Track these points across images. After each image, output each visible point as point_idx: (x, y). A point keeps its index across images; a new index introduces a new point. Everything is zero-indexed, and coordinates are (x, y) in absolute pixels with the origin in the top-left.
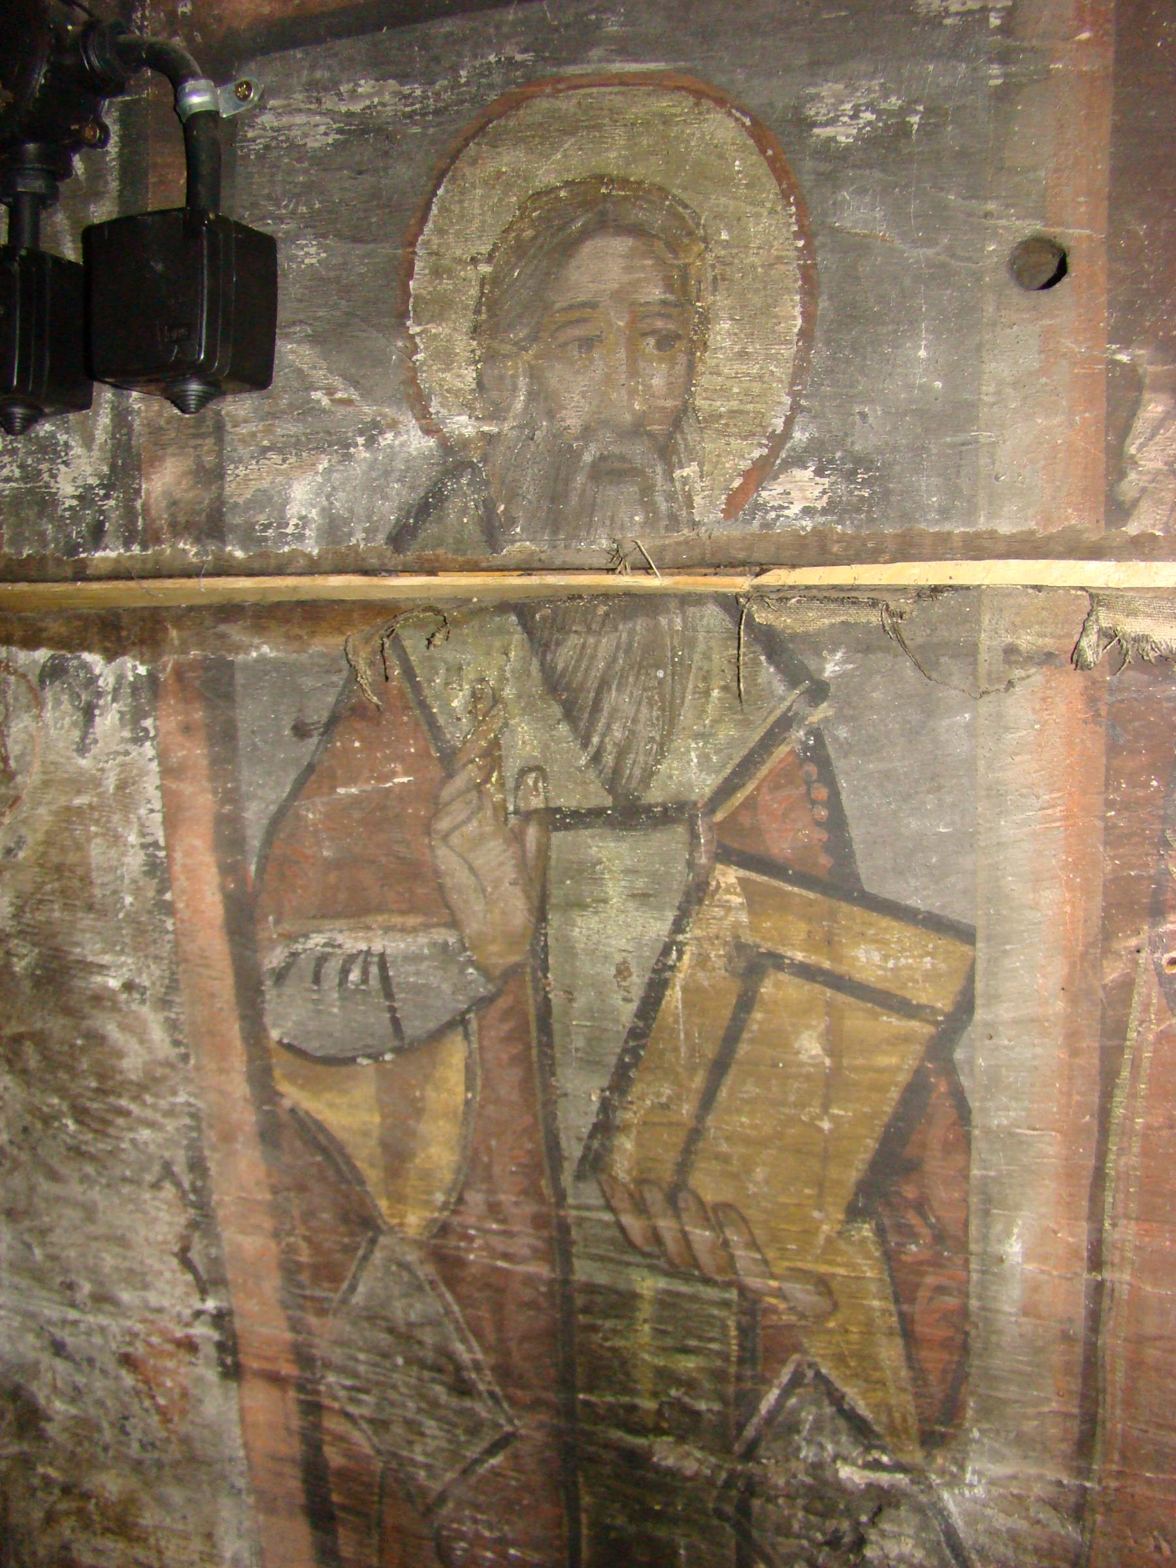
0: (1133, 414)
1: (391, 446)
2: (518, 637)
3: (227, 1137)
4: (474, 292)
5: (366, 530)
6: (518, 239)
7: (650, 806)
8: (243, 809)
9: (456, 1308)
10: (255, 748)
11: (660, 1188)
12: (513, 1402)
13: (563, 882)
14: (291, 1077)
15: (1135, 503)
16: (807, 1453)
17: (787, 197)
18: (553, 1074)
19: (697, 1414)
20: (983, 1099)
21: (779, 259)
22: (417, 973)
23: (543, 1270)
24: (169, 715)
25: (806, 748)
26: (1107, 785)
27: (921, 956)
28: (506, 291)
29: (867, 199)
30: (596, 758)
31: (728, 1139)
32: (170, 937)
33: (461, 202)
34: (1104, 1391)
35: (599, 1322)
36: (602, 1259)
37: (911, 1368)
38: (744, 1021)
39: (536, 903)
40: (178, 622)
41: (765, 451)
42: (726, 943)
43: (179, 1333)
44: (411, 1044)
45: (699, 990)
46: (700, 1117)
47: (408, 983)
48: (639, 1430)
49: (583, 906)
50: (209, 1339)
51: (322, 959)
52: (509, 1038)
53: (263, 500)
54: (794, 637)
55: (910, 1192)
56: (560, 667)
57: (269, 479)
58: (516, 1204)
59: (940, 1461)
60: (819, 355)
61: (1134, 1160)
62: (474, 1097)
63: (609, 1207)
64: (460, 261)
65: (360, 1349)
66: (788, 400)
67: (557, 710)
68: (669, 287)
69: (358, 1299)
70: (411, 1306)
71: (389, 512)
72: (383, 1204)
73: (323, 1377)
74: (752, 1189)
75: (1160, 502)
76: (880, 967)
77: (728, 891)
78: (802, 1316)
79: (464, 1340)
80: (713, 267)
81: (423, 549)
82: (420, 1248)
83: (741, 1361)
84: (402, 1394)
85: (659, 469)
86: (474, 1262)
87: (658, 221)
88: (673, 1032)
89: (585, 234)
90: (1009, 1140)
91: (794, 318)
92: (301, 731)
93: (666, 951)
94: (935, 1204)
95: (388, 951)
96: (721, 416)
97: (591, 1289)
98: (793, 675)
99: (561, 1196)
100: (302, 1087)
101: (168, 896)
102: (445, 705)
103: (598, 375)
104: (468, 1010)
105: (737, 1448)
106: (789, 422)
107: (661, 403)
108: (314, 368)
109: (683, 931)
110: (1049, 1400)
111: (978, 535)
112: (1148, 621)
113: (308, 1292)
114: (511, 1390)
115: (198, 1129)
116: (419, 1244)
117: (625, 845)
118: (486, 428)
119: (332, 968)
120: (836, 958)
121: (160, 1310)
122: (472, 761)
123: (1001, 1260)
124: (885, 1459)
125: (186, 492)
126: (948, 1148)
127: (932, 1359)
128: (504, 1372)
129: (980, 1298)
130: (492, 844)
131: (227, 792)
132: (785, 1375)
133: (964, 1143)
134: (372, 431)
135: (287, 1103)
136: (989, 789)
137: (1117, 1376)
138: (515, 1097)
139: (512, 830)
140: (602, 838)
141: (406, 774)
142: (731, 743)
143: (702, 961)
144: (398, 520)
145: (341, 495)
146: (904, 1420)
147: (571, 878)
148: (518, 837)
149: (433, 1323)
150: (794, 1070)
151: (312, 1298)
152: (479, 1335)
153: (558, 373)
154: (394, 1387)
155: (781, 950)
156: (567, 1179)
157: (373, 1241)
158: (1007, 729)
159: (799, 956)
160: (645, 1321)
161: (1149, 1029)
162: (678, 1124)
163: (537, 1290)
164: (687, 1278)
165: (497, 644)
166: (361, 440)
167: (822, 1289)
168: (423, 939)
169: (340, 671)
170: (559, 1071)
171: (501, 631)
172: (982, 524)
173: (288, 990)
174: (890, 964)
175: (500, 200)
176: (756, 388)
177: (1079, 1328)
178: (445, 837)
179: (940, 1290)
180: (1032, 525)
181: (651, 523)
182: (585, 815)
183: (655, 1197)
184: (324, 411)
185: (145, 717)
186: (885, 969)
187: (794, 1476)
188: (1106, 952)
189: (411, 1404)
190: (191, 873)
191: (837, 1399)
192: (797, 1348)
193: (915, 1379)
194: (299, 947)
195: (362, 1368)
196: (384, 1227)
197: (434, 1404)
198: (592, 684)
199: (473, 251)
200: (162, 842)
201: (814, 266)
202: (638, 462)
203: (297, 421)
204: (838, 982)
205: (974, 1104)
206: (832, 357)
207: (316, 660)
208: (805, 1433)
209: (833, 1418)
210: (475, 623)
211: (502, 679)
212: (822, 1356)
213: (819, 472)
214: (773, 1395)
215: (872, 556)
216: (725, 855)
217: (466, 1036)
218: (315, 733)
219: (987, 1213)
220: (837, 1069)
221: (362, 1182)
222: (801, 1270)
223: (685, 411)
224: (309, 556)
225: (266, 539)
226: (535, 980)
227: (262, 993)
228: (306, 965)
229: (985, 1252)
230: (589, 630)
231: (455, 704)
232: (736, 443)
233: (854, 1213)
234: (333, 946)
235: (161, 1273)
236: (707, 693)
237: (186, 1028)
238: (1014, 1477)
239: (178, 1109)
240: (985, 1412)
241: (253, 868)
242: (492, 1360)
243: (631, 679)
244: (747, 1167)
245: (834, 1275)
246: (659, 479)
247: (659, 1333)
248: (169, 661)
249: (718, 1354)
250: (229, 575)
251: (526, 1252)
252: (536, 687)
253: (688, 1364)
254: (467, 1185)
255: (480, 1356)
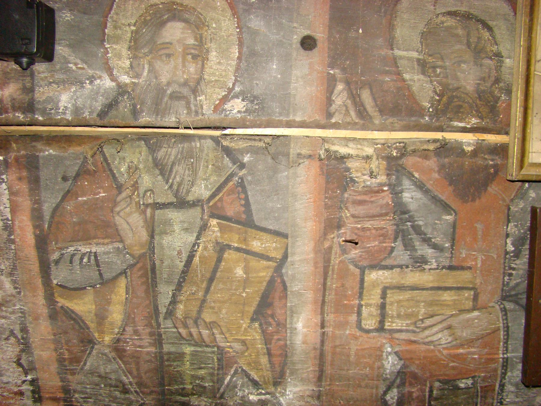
0: (334, 88)
1: (99, 84)
2: (144, 149)
3: (36, 319)
4: (129, 35)
5: (89, 112)
6: (145, 19)
7: (189, 201)
8: (42, 206)
9: (123, 366)
10: (47, 185)
11: (192, 319)
12: (143, 393)
13: (159, 226)
14: (61, 296)
15: (334, 113)
16: (240, 394)
17: (234, 16)
18: (156, 287)
19: (205, 387)
20: (291, 283)
21: (231, 34)
22: (108, 258)
23: (152, 349)
24: (12, 174)
25: (238, 183)
26: (325, 192)
27: (272, 243)
28: (141, 36)
29: (259, 19)
30: (171, 187)
31: (214, 302)
32: (13, 251)
33: (124, 5)
34: (325, 362)
35: (172, 363)
36: (173, 343)
37: (270, 364)
38: (219, 266)
39: (150, 233)
40: (16, 142)
41: (226, 93)
42: (213, 242)
43: (16, 389)
44: (106, 281)
45: (204, 257)
46: (205, 296)
47: (105, 261)
48: (187, 395)
49: (167, 234)
50: (28, 390)
51: (73, 255)
52: (141, 277)
53: (50, 100)
54: (235, 150)
55: (269, 312)
56: (159, 158)
57: (52, 93)
58: (143, 329)
59: (279, 389)
60: (243, 65)
61: (333, 297)
62: (129, 296)
63: (176, 327)
64: (124, 25)
65: (88, 384)
66: (234, 78)
67: (157, 172)
68: (196, 40)
69: (87, 367)
70: (106, 367)
71: (98, 106)
72: (96, 335)
73: (73, 396)
74: (222, 316)
75: (341, 113)
76: (260, 247)
77: (214, 226)
78: (237, 353)
79: (126, 376)
80: (210, 35)
81: (111, 119)
82: (110, 348)
83: (218, 369)
84: (103, 397)
85: (192, 97)
86: (129, 350)
87: (193, 19)
88: (196, 271)
89: (168, 20)
90: (298, 294)
91: (236, 53)
92: (65, 179)
93: (194, 246)
94: (277, 315)
95: (98, 251)
96: (212, 81)
97: (169, 353)
98: (234, 161)
99: (159, 325)
100: (66, 299)
101: (12, 237)
102: (119, 170)
103: (172, 66)
104: (127, 269)
105: (218, 395)
106: (234, 84)
107: (193, 76)
108: (70, 56)
109: (200, 239)
110: (310, 367)
111: (290, 121)
112: (338, 147)
113: (68, 368)
114: (142, 390)
115: (25, 317)
116: (109, 346)
117: (180, 214)
118: (133, 81)
119: (77, 258)
120: (247, 245)
121: (7, 383)
122: (128, 188)
123: (296, 329)
124: (263, 391)
125: (19, 96)
126: (280, 298)
127: (276, 360)
128: (140, 384)
129: (290, 340)
130: (135, 215)
131: (36, 200)
132: (232, 372)
133: (285, 297)
134: (92, 79)
135: (60, 305)
136: (293, 194)
137: (329, 358)
138: (143, 295)
139: (142, 210)
140: (173, 212)
141: (104, 193)
142: (215, 181)
143: (205, 248)
144: (101, 109)
145: (80, 100)
146: (268, 379)
147: (162, 225)
148: (144, 212)
149: (114, 372)
150: (234, 279)
151: (70, 370)
152: (131, 373)
153: (158, 65)
154: (100, 395)
155: (230, 244)
156: (161, 319)
157: (93, 347)
158: (298, 177)
159: (236, 245)
160: (188, 361)
161: (337, 260)
162: (198, 299)
163: (151, 356)
164: (200, 346)
165: (137, 150)
166: (88, 82)
167: (243, 344)
168: (110, 247)
169: (80, 159)
170: (158, 285)
171: (139, 146)
172: (291, 118)
173: (61, 266)
174: (263, 246)
175: (139, 6)
176: (224, 73)
177: (318, 346)
178: (118, 213)
179: (279, 340)
180: (306, 119)
181: (189, 113)
182: (167, 205)
183: (190, 322)
184: (74, 71)
185: (3, 174)
186: (262, 247)
187: (236, 401)
188: (325, 239)
189: (107, 399)
190: (21, 228)
191: (248, 376)
192: (236, 362)
193: (271, 367)
194: (64, 252)
195: (88, 390)
196: (97, 342)
197: (115, 398)
198: (170, 164)
199: (129, 22)
200: (10, 218)
201: (242, 37)
202: (185, 94)
203: (63, 74)
204: (247, 252)
205: (288, 285)
206: (248, 66)
207: (71, 155)
208: (239, 388)
209: (247, 382)
210: (130, 144)
211: (139, 162)
212: (244, 364)
213: (243, 100)
214: (229, 378)
215: (259, 126)
216: (213, 216)
217: (126, 277)
218: (71, 180)
219: (292, 316)
220: (247, 278)
221: (88, 328)
222: (236, 339)
223: (201, 79)
224: (68, 120)
225: (51, 114)
226: (150, 257)
227: (50, 268)
228: (67, 258)
229: (291, 327)
230: (169, 147)
231: (122, 170)
232: (217, 90)
233: (253, 320)
234: (77, 251)
235: (9, 369)
236: (207, 167)
237: (20, 283)
238: (301, 391)
239: (16, 311)
240: (292, 374)
241: (47, 226)
242: (136, 380)
243: (183, 162)
244: (220, 310)
245: (247, 339)
246: (192, 100)
247: (192, 364)
248: (13, 155)
249: (211, 368)
250: (36, 125)
251: (147, 344)
252: (151, 164)
253: (202, 372)
254: (126, 325)
255: (131, 380)
